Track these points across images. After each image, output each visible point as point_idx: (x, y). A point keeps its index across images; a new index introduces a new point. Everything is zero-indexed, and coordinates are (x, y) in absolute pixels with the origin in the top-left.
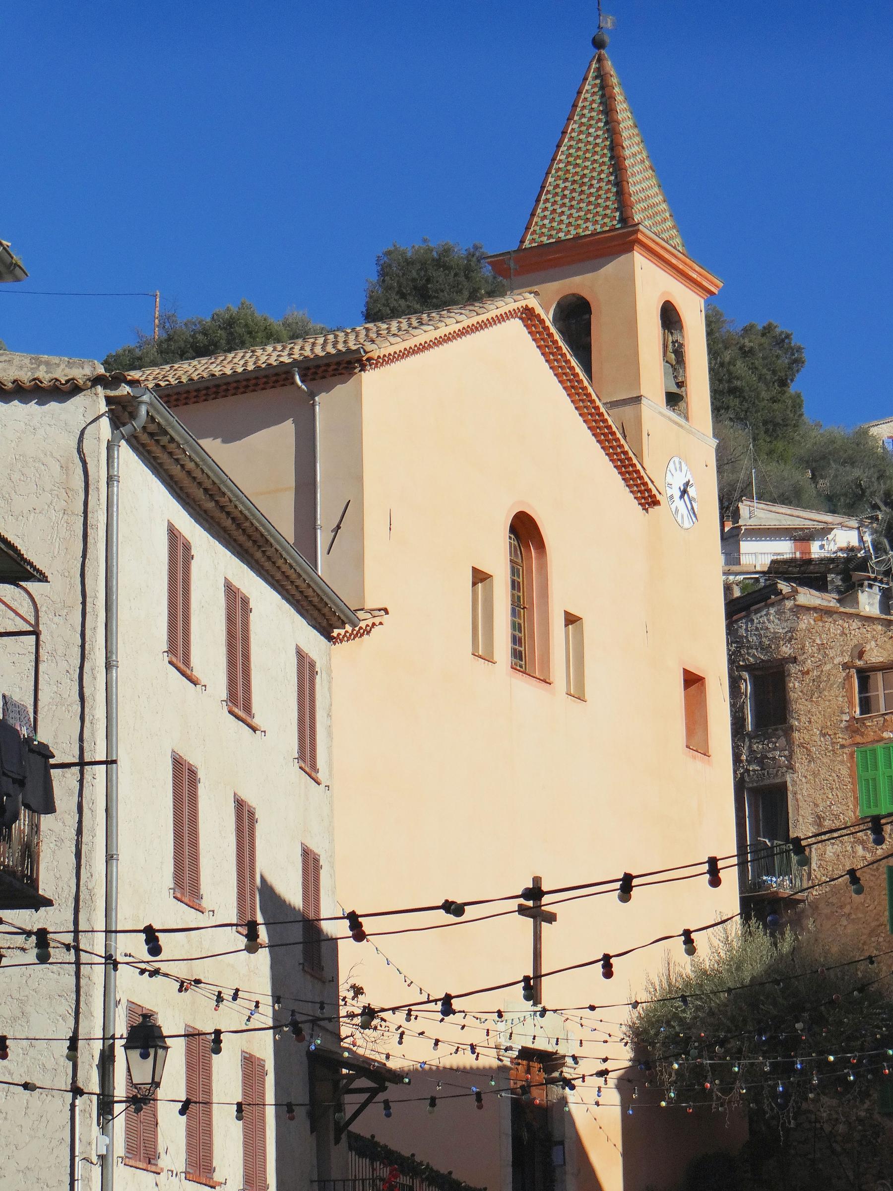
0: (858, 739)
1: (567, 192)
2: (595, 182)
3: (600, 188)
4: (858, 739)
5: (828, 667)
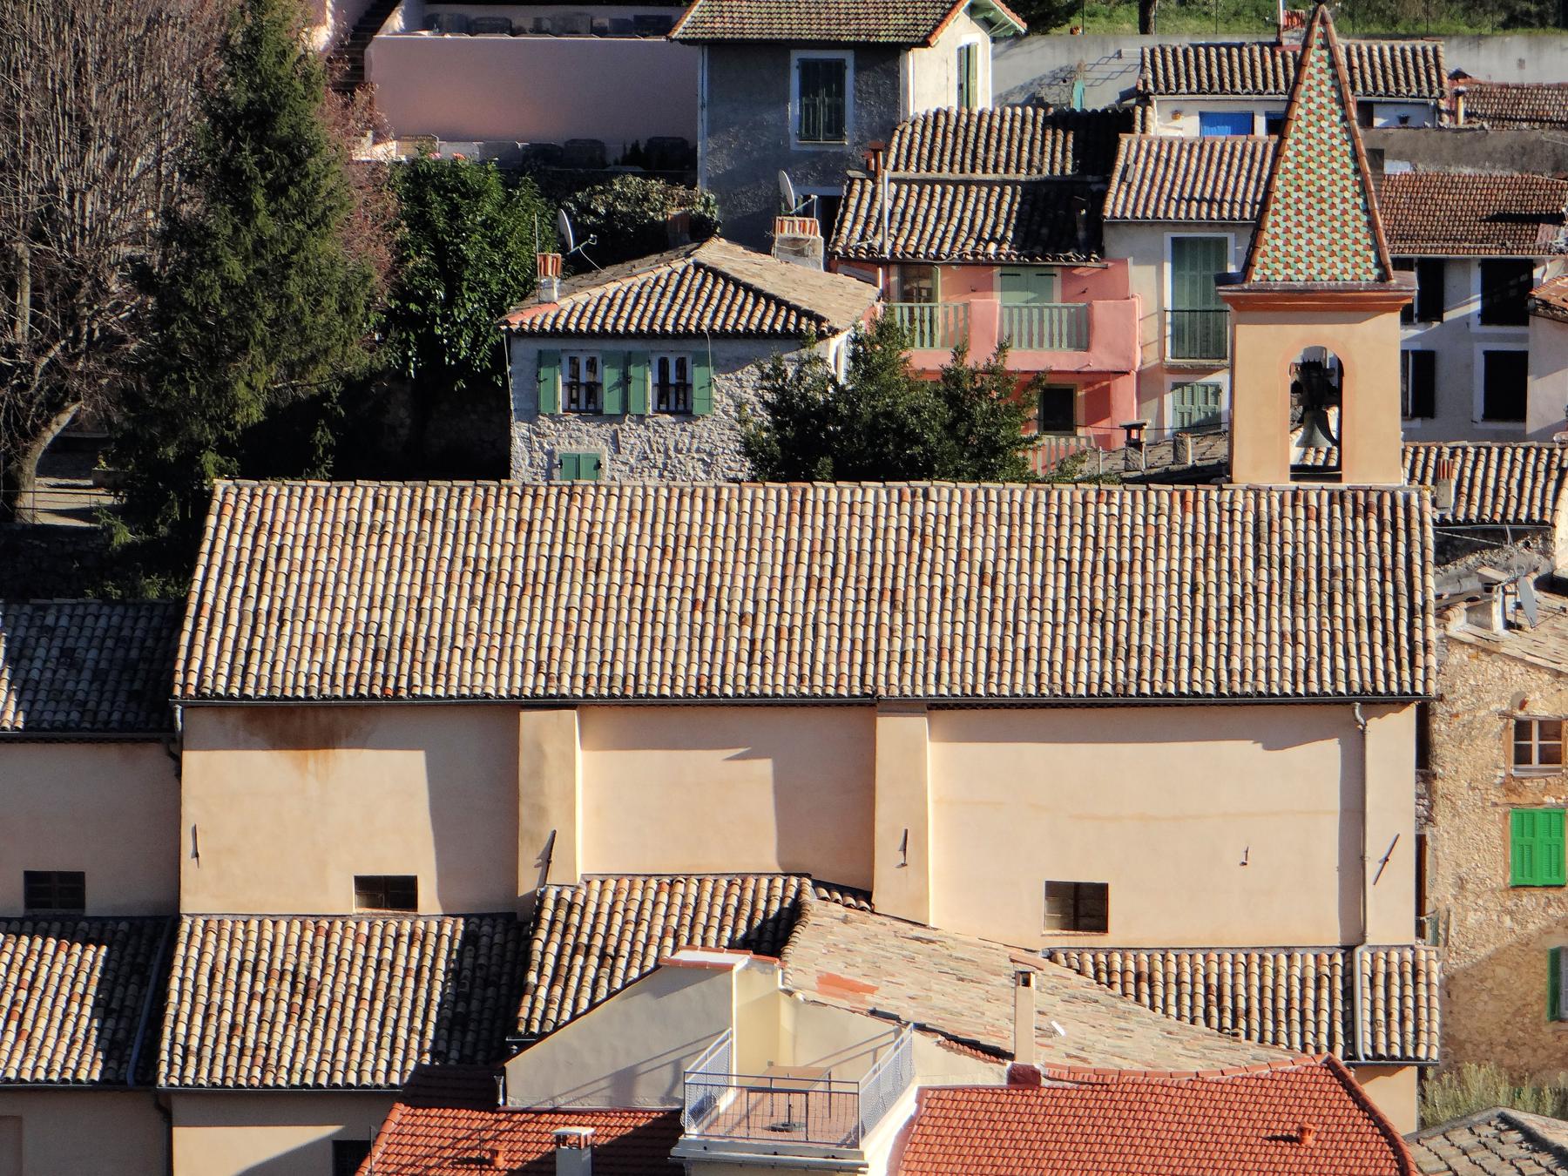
0: (1514, 799)
1: (1302, 207)
2: (1337, 201)
3: (1344, 212)
4: (1514, 799)
5: (1483, 713)
